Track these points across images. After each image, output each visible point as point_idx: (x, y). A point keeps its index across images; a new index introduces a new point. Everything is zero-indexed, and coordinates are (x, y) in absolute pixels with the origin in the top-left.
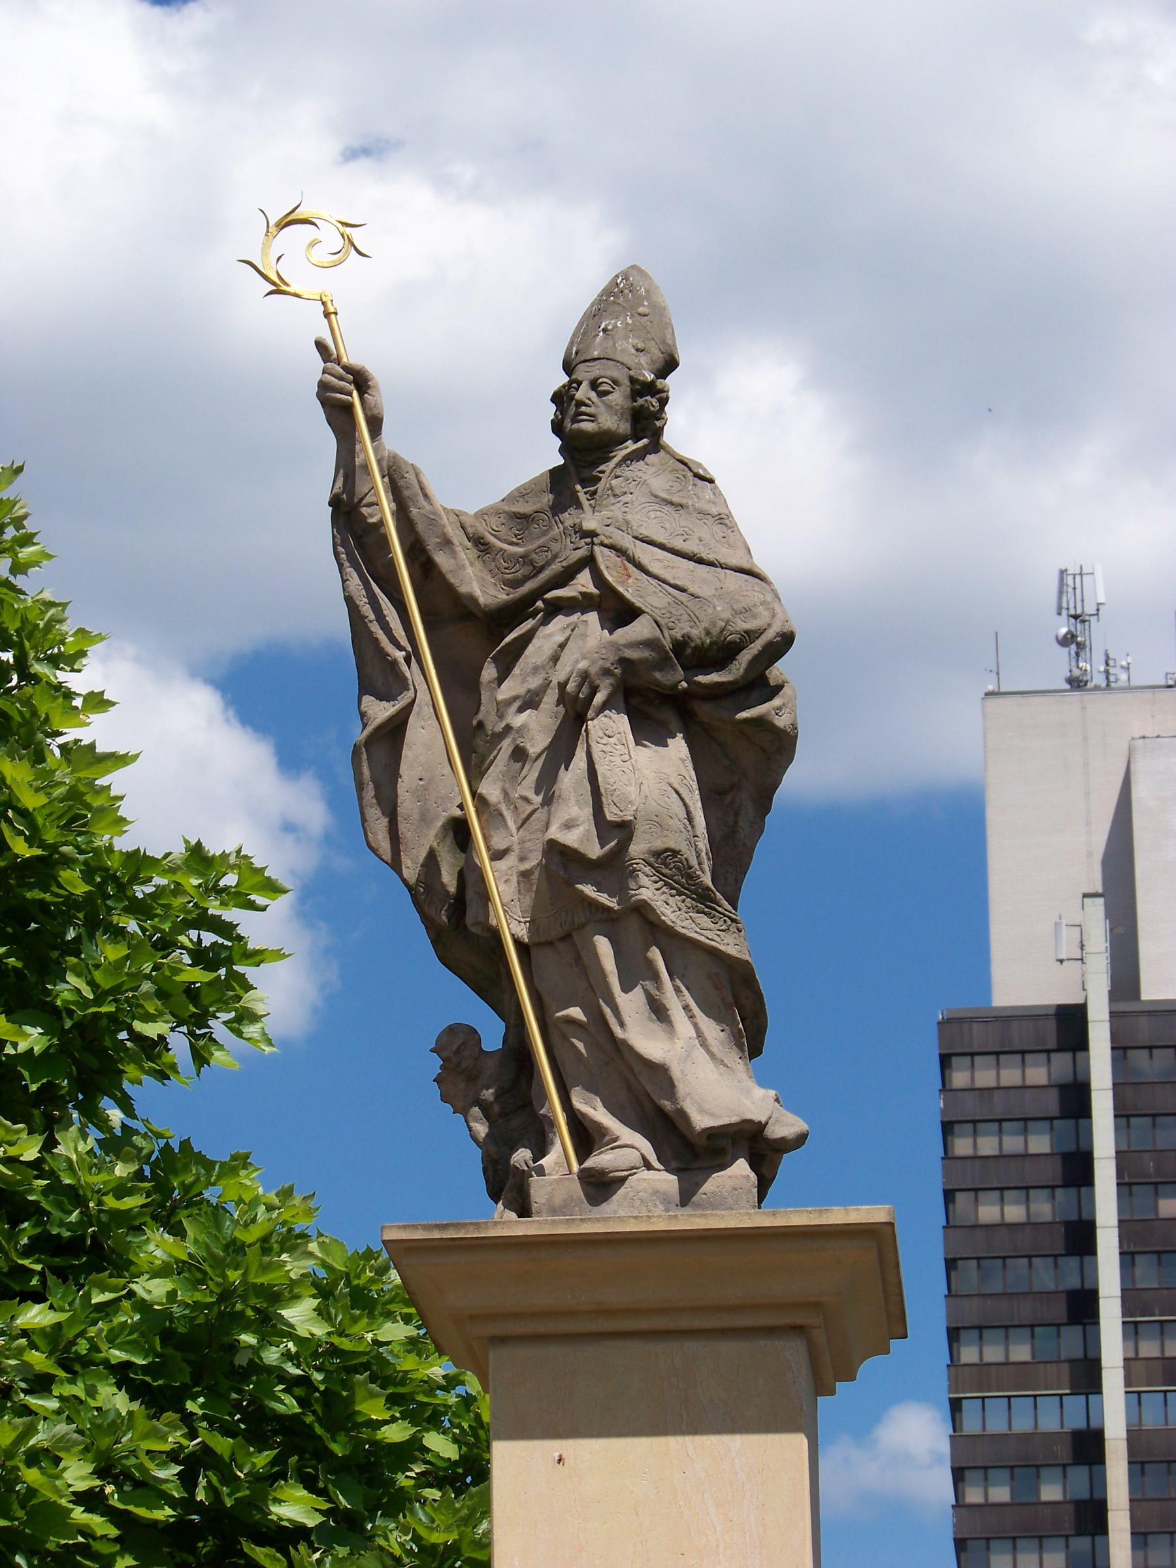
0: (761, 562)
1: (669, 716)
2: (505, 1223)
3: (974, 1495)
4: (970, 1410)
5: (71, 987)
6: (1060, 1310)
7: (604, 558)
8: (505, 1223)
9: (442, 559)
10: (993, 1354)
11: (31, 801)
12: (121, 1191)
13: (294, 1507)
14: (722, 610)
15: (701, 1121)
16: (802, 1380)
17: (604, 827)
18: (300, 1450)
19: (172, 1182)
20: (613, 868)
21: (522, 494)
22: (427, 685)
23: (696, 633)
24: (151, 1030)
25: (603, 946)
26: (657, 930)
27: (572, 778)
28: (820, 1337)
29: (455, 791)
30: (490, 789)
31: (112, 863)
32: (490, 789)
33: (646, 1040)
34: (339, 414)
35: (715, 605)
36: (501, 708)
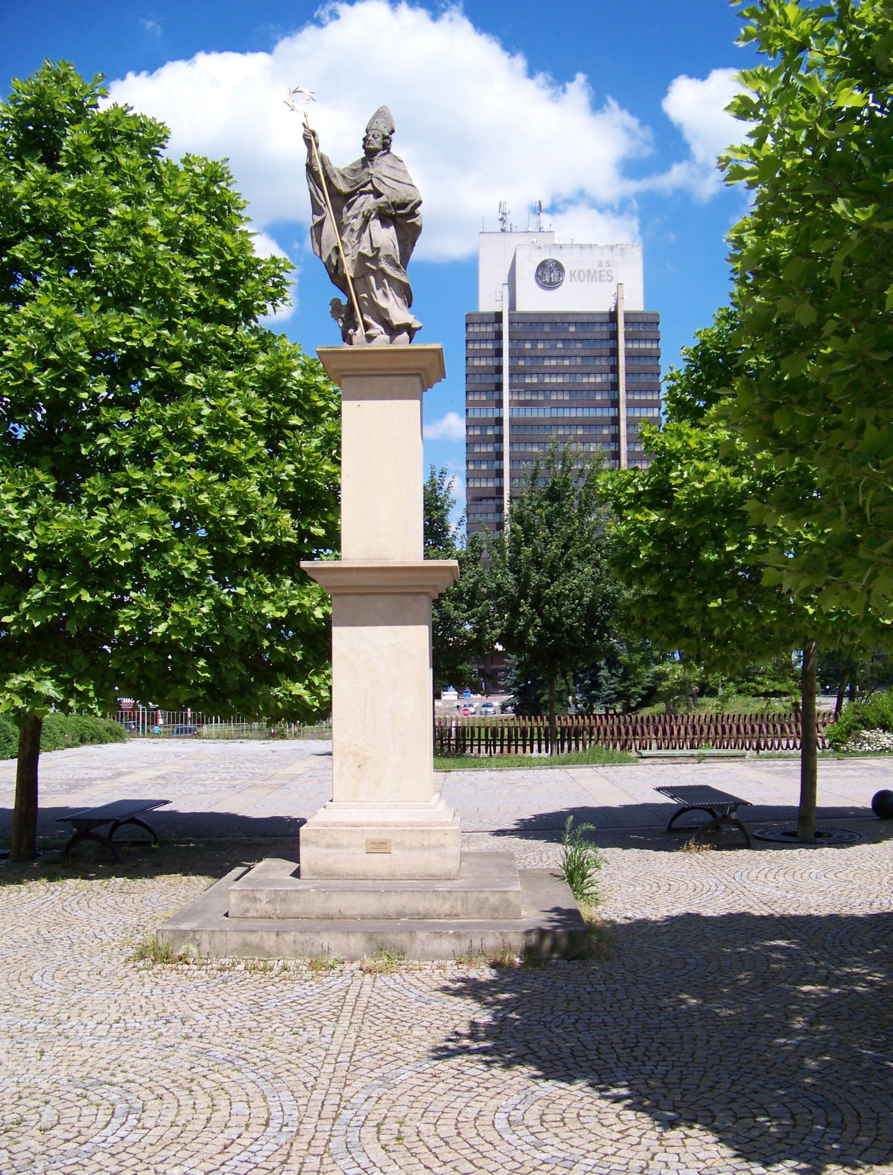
0: (414, 183)
1: (390, 221)
2: (346, 347)
3: (471, 433)
4: (470, 412)
5: (241, 293)
6: (493, 388)
7: (374, 180)
8: (346, 347)
9: (333, 180)
10: (477, 398)
11: (231, 245)
12: (253, 343)
13: (295, 421)
14: (404, 195)
15: (395, 323)
16: (419, 387)
17: (373, 249)
18: (296, 407)
19: (266, 341)
20: (375, 259)
21: (354, 164)
22: (329, 212)
23: (398, 200)
24: (261, 303)
25: (372, 279)
26: (385, 275)
27: (365, 236)
28: (423, 376)
29: (336, 240)
30: (344, 239)
31: (252, 261)
32: (344, 239)
33: (381, 302)
34: (308, 142)
35: (402, 194)
36: (348, 218)
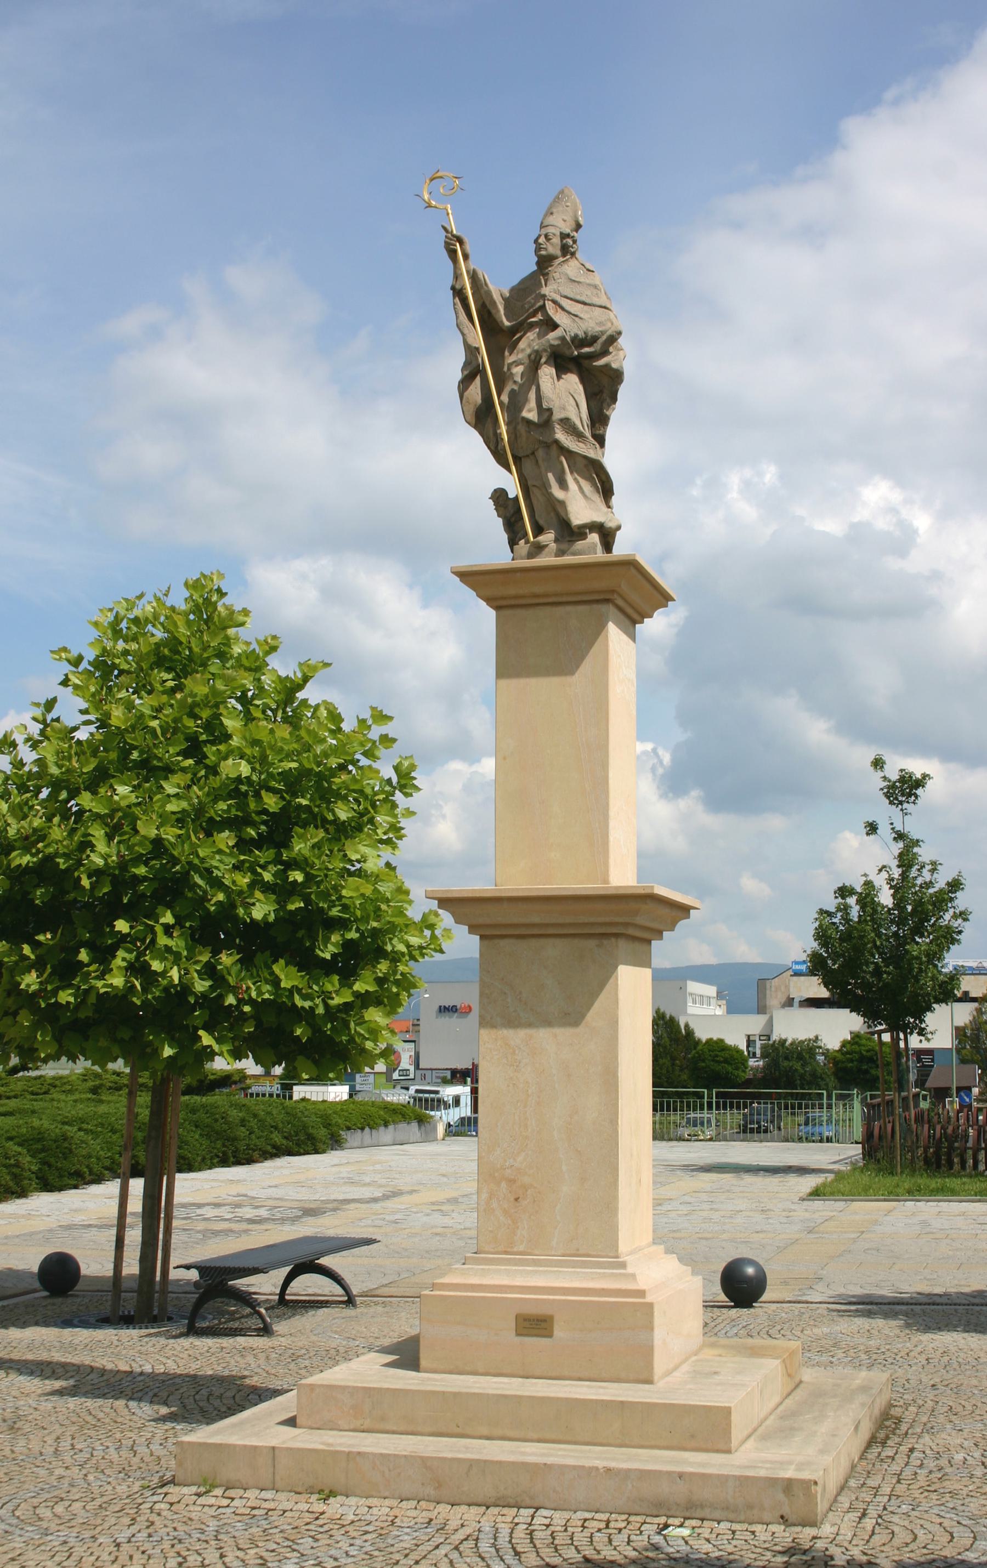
1: (571, 366)
7: (550, 307)
34: (452, 254)
